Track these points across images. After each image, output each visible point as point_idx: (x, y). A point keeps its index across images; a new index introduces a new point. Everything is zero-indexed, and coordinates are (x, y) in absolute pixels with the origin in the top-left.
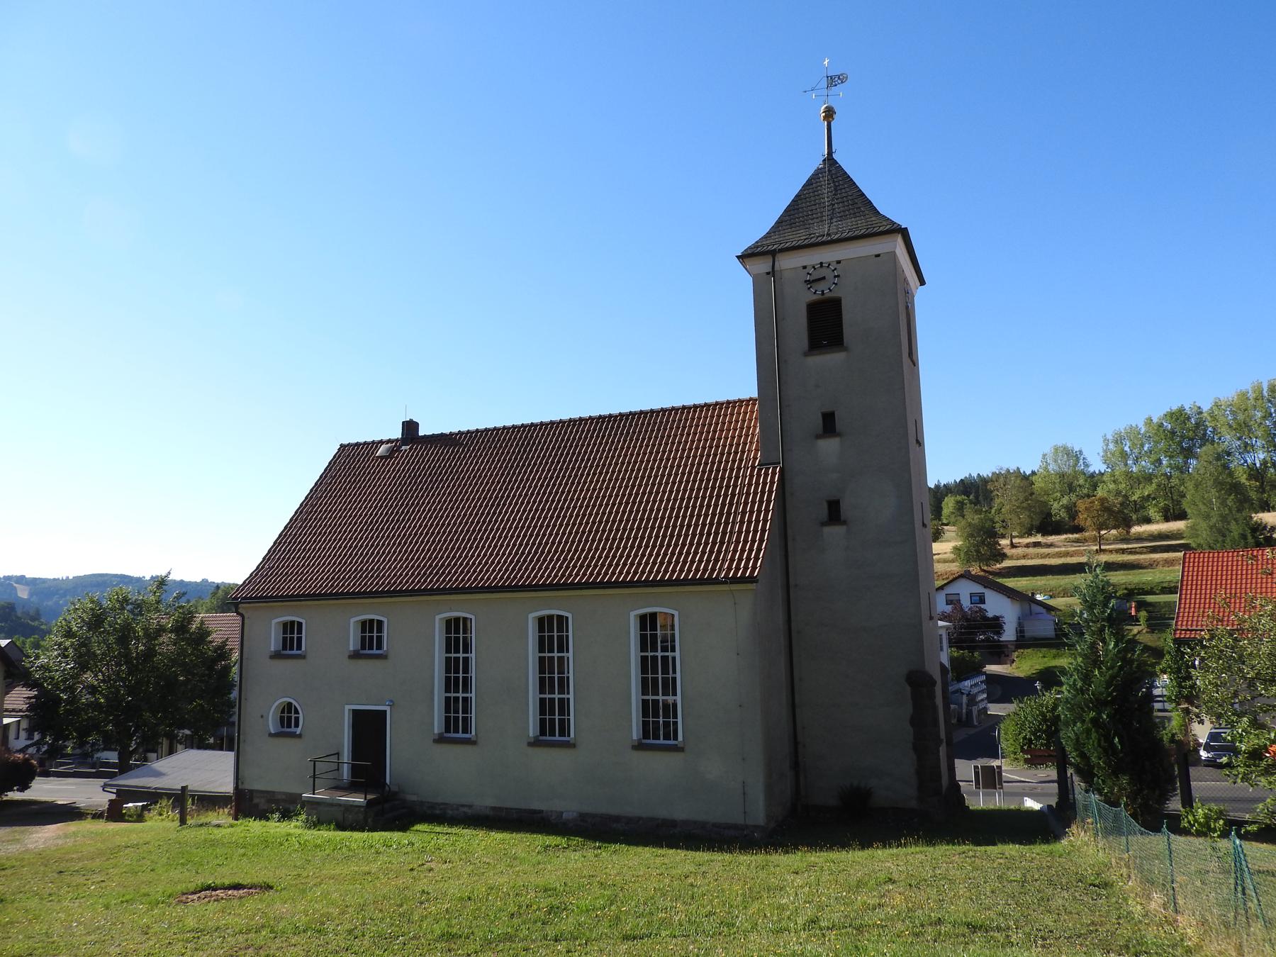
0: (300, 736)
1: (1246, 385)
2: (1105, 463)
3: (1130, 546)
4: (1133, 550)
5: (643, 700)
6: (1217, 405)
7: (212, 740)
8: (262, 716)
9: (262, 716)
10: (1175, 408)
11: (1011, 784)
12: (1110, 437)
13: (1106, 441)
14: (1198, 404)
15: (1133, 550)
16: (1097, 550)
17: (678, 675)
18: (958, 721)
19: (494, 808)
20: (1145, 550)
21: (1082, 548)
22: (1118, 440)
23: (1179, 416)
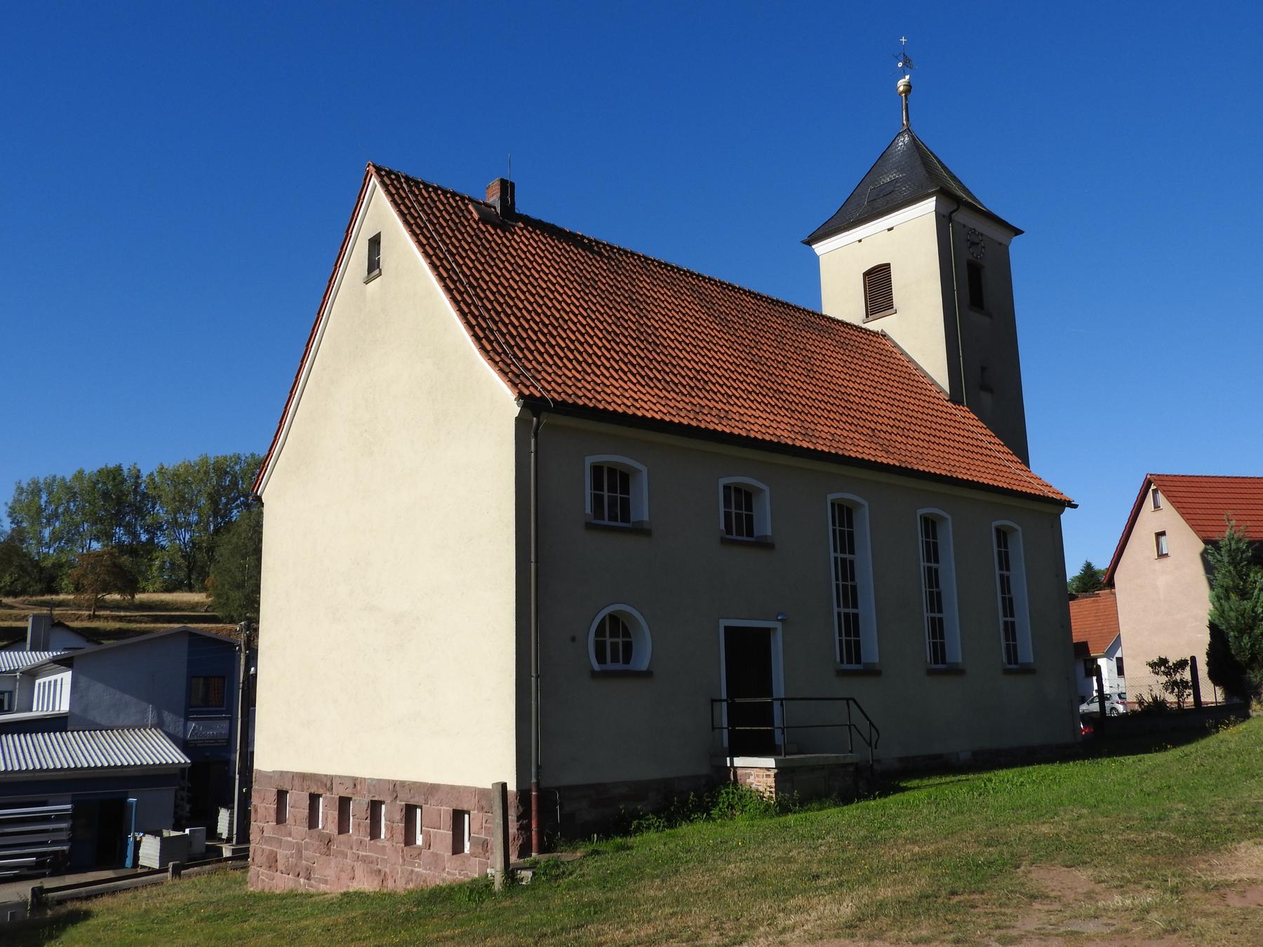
0: (647, 674)
1: (194, 458)
2: (9, 516)
3: (128, 614)
4: (132, 618)
5: (857, 608)
6: (162, 471)
7: (226, 768)
8: (573, 639)
9: (573, 639)
10: (111, 465)
11: (849, 741)
12: (24, 485)
13: (20, 490)
14: (138, 467)
15: (132, 618)
16: (89, 615)
17: (834, 583)
18: (1071, 594)
19: (901, 759)
20: (146, 618)
21: (70, 612)
22: (36, 491)
23: (115, 474)
